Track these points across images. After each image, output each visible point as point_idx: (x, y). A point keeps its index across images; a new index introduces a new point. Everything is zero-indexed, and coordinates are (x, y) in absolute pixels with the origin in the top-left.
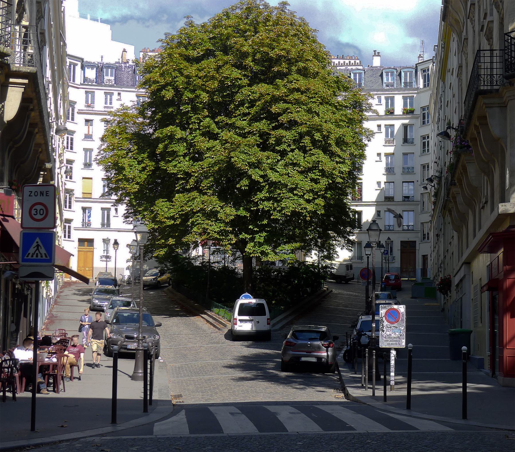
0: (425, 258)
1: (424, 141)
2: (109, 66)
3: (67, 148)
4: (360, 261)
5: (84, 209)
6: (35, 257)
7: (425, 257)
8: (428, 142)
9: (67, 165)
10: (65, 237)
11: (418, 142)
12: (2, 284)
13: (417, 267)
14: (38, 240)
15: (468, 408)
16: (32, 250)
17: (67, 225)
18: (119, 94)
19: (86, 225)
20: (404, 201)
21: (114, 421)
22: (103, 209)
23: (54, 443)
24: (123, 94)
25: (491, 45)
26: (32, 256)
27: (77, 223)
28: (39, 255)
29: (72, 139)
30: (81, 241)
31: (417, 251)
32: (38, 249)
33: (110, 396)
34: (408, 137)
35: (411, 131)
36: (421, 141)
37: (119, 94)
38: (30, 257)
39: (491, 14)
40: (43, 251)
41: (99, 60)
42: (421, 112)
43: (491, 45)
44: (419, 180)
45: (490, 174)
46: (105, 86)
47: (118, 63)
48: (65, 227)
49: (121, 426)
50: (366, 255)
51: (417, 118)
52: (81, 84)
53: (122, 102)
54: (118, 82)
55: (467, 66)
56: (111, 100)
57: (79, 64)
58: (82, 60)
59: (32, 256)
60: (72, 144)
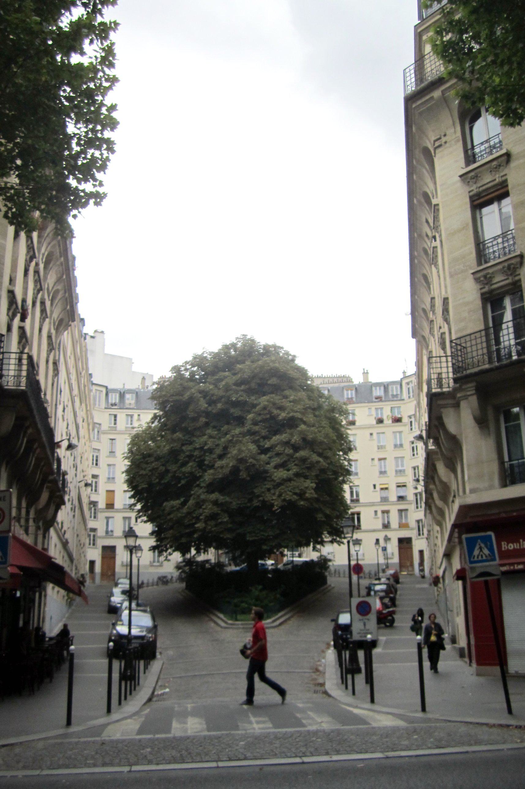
2: (130, 391)
3: (91, 517)
5: (108, 518)
6: (480, 557)
7: (421, 552)
14: (479, 541)
15: (74, 713)
16: (476, 552)
17: (92, 534)
18: (139, 415)
21: (69, 723)
22: (125, 518)
23: (12, 745)
24: (142, 416)
25: (445, 352)
26: (478, 557)
28: (484, 556)
30: (105, 548)
32: (481, 550)
37: (139, 415)
38: (476, 559)
39: (444, 327)
40: (486, 551)
41: (121, 387)
43: (445, 352)
45: (454, 471)
46: (127, 409)
47: (138, 388)
48: (89, 536)
49: (73, 729)
50: (356, 551)
52: (106, 408)
53: (140, 423)
54: (139, 406)
55: (69, 379)
56: (132, 421)
58: (106, 387)
59: (478, 557)
60: (97, 460)
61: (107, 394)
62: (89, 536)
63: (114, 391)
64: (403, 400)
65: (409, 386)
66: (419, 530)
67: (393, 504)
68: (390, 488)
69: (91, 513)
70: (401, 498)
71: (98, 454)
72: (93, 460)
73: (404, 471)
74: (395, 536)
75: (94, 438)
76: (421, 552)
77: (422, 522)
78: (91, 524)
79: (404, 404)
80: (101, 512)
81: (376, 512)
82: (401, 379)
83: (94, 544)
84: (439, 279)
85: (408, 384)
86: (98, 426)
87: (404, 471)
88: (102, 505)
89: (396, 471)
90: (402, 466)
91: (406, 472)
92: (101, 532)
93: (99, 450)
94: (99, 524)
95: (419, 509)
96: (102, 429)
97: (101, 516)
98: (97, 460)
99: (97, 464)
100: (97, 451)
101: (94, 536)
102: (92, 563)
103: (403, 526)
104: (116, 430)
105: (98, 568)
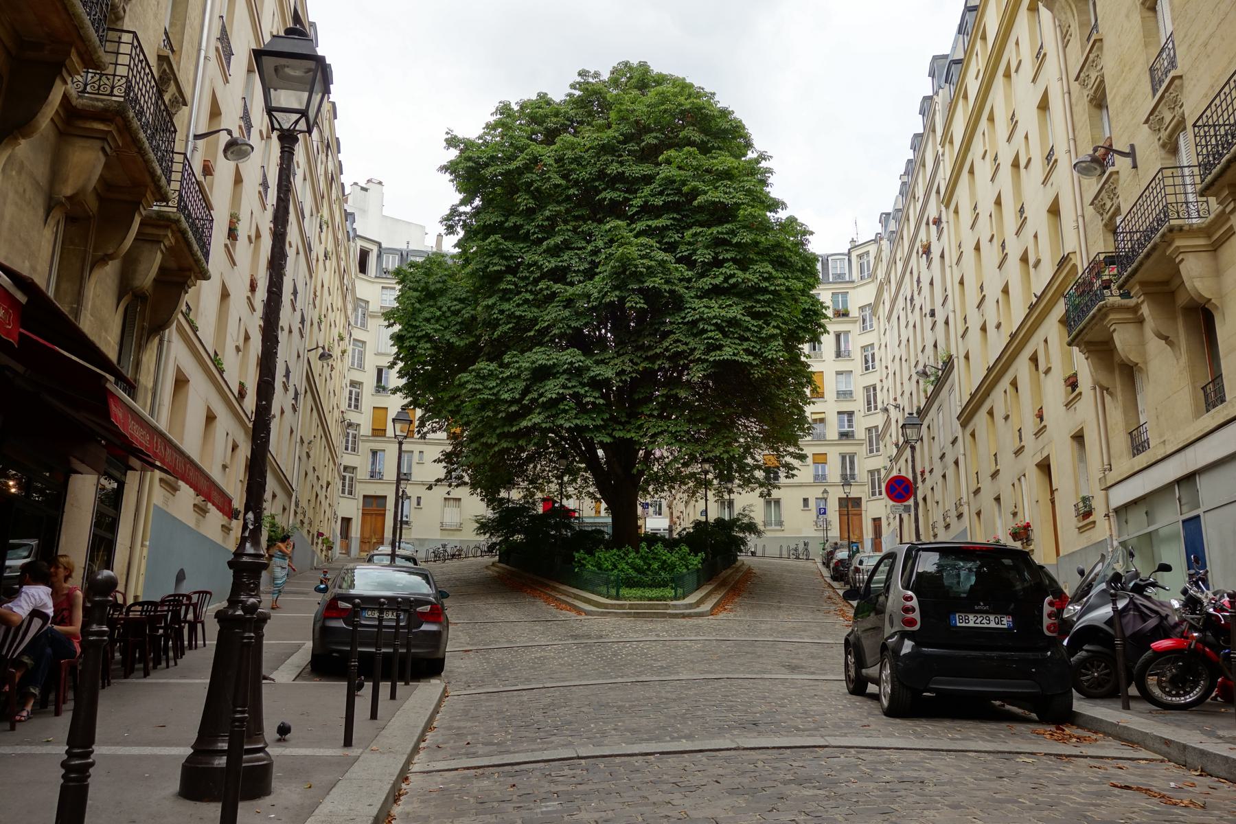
0: (877, 522)
1: (865, 354)
3: (347, 449)
4: (779, 528)
5: (374, 453)
8: (873, 355)
9: (352, 389)
10: (343, 492)
11: (857, 355)
12: (601, 601)
13: (865, 537)
17: (348, 475)
19: (375, 475)
20: (840, 439)
27: (363, 473)
29: (358, 394)
31: (863, 513)
33: (125, 28)
34: (843, 349)
35: (847, 341)
36: (862, 354)
41: (404, 247)
42: (860, 314)
44: (862, 410)
48: (344, 478)
51: (855, 322)
52: (376, 277)
57: (375, 249)
58: (379, 244)
60: (357, 400)
61: (379, 256)
62: (344, 478)
63: (392, 251)
64: (853, 282)
65: (862, 261)
66: (873, 487)
67: (832, 444)
68: (828, 421)
69: (347, 442)
70: (844, 435)
71: (358, 390)
72: (350, 399)
73: (851, 393)
74: (836, 494)
75: (356, 323)
76: (877, 522)
77: (877, 431)
78: (348, 459)
79: (854, 288)
80: (363, 441)
81: (806, 501)
82: (849, 250)
83: (350, 493)
84: (919, 278)
85: (860, 256)
86: (363, 305)
87: (851, 393)
88: (366, 430)
89: (838, 393)
90: (850, 426)
91: (854, 395)
92: (363, 473)
93: (364, 343)
94: (360, 461)
95: (873, 411)
96: (370, 310)
97: (365, 447)
98: (357, 400)
99: (356, 407)
100: (360, 344)
101: (351, 479)
102: (346, 521)
103: (847, 480)
104: (385, 436)
105: (355, 531)
